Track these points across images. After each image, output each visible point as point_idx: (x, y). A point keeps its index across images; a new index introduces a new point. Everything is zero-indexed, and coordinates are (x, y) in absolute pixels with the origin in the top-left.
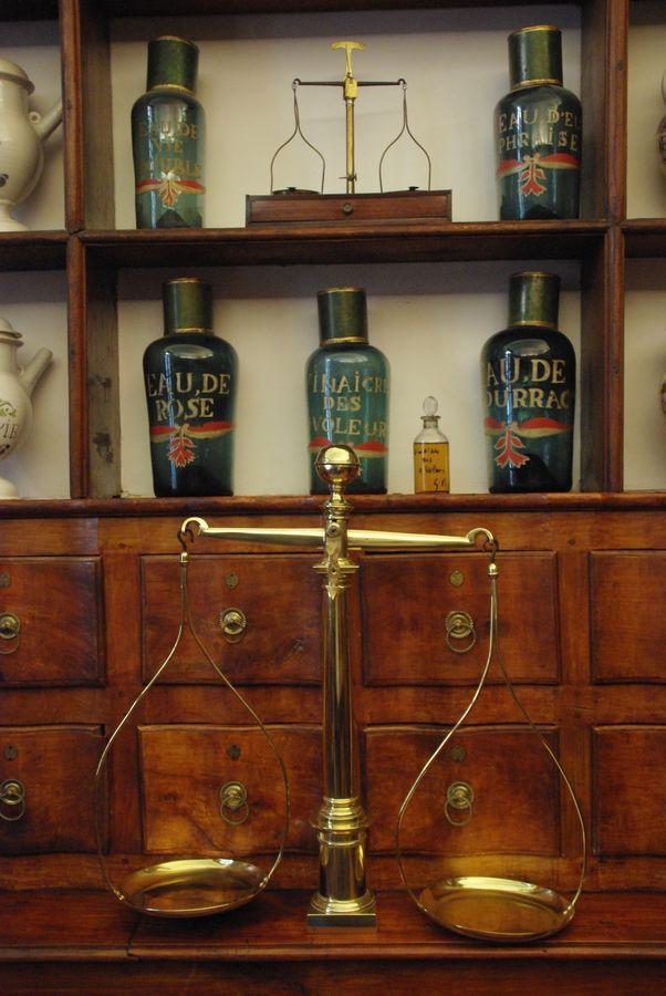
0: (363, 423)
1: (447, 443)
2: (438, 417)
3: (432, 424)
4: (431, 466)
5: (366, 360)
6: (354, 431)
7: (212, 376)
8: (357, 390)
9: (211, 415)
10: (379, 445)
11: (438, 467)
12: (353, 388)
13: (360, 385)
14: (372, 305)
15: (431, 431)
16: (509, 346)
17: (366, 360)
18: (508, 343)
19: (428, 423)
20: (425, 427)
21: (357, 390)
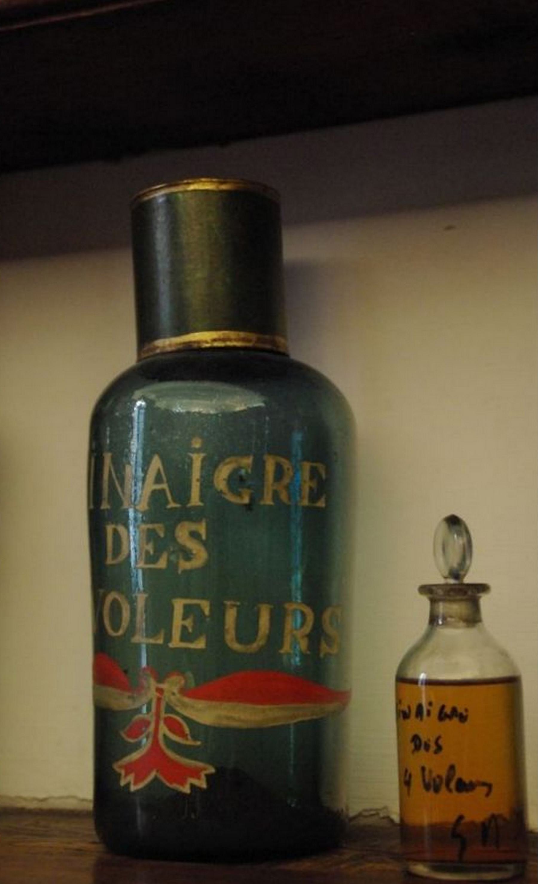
0: (219, 611)
1: (512, 683)
2: (483, 588)
3: (457, 608)
4: (437, 766)
5: (257, 402)
6: (185, 636)
7: (282, 460)
8: (195, 500)
9: (200, 644)
10: (315, 680)
11: (464, 773)
12: (181, 490)
13: (207, 483)
14: (297, 247)
15: (454, 634)
16: (138, 393)
17: (257, 402)
18: (143, 386)
19: (442, 608)
20: (433, 620)
21: (195, 500)
